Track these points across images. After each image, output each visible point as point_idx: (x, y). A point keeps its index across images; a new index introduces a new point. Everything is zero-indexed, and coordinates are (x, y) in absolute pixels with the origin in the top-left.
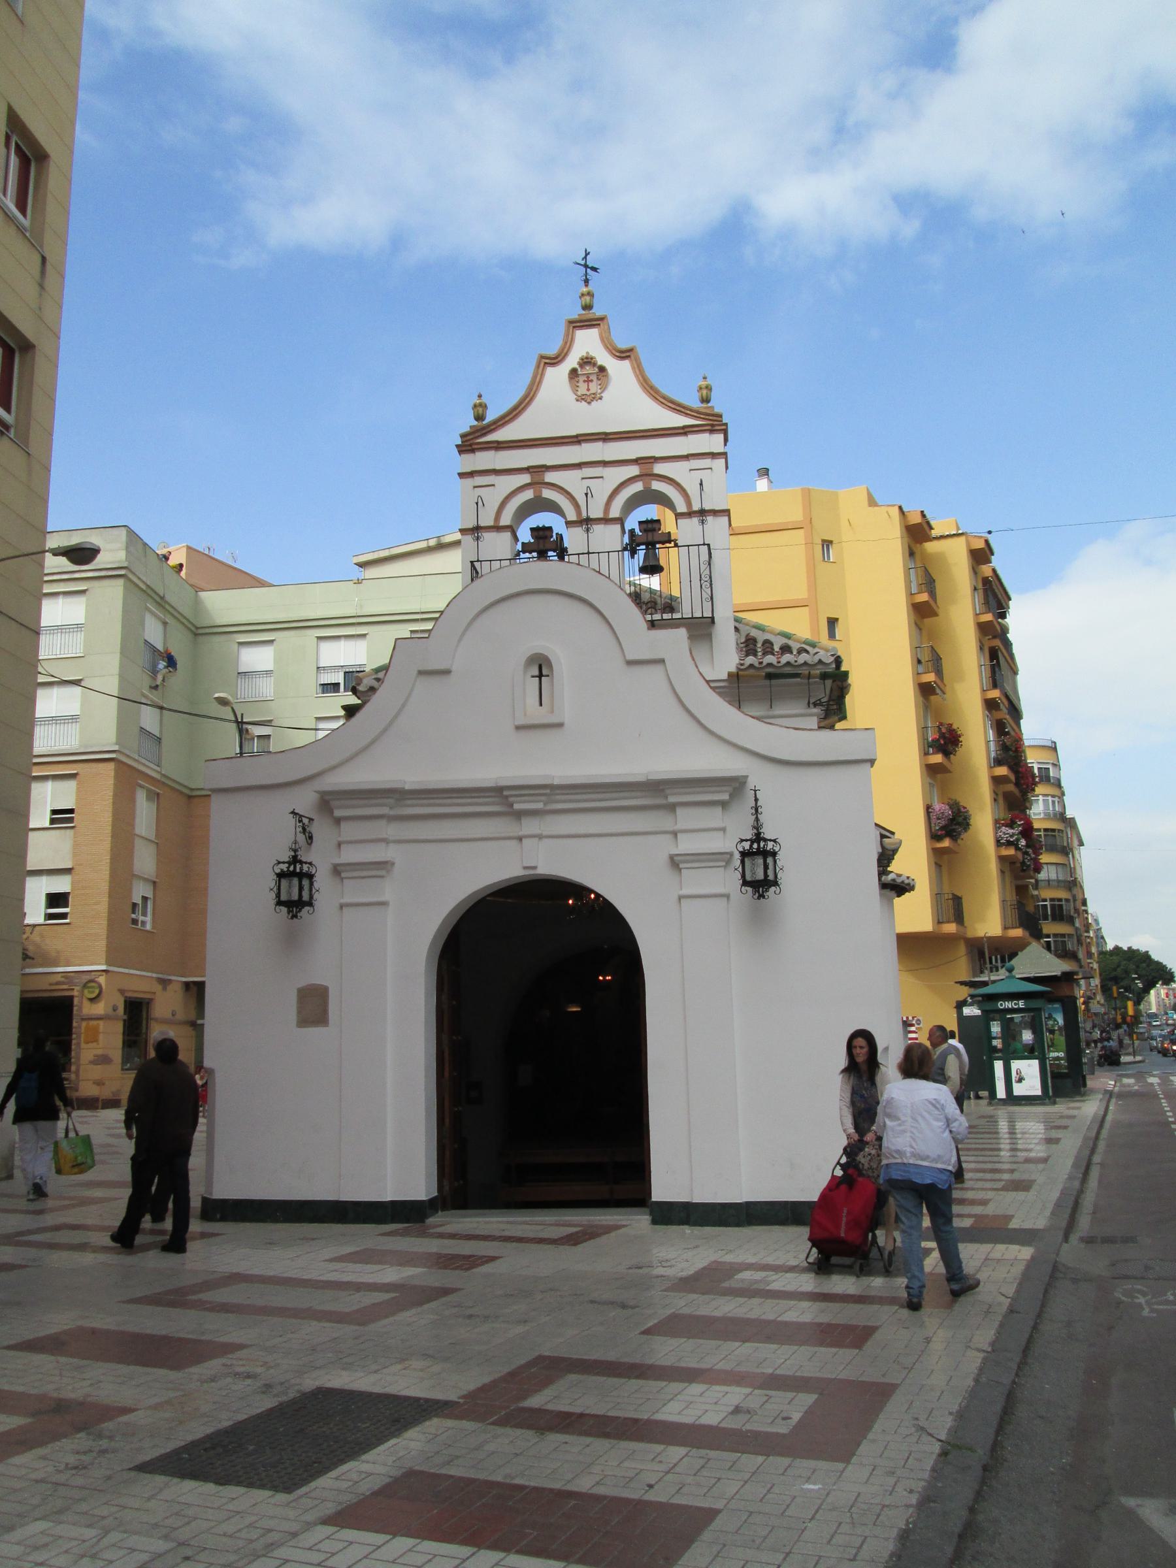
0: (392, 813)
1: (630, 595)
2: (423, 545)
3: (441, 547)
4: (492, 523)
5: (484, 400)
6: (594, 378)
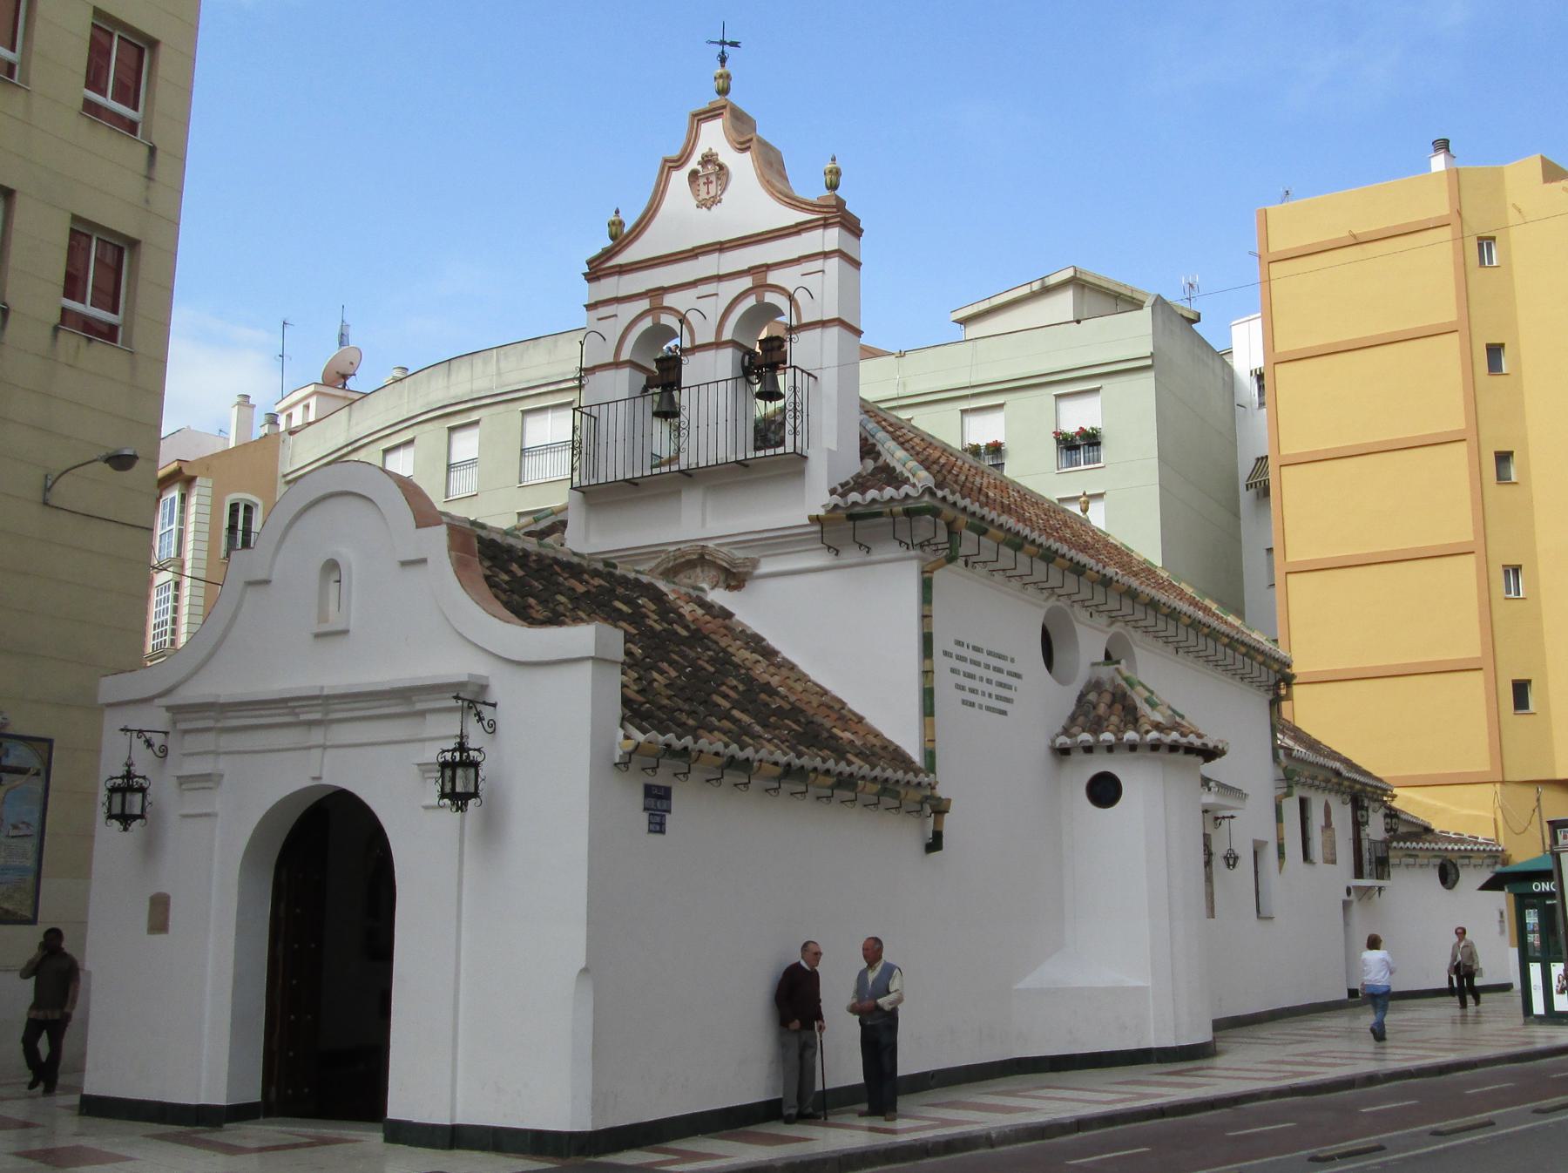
0: (219, 725)
3: (1047, 290)
4: (611, 360)
5: (838, 164)
6: (713, 178)
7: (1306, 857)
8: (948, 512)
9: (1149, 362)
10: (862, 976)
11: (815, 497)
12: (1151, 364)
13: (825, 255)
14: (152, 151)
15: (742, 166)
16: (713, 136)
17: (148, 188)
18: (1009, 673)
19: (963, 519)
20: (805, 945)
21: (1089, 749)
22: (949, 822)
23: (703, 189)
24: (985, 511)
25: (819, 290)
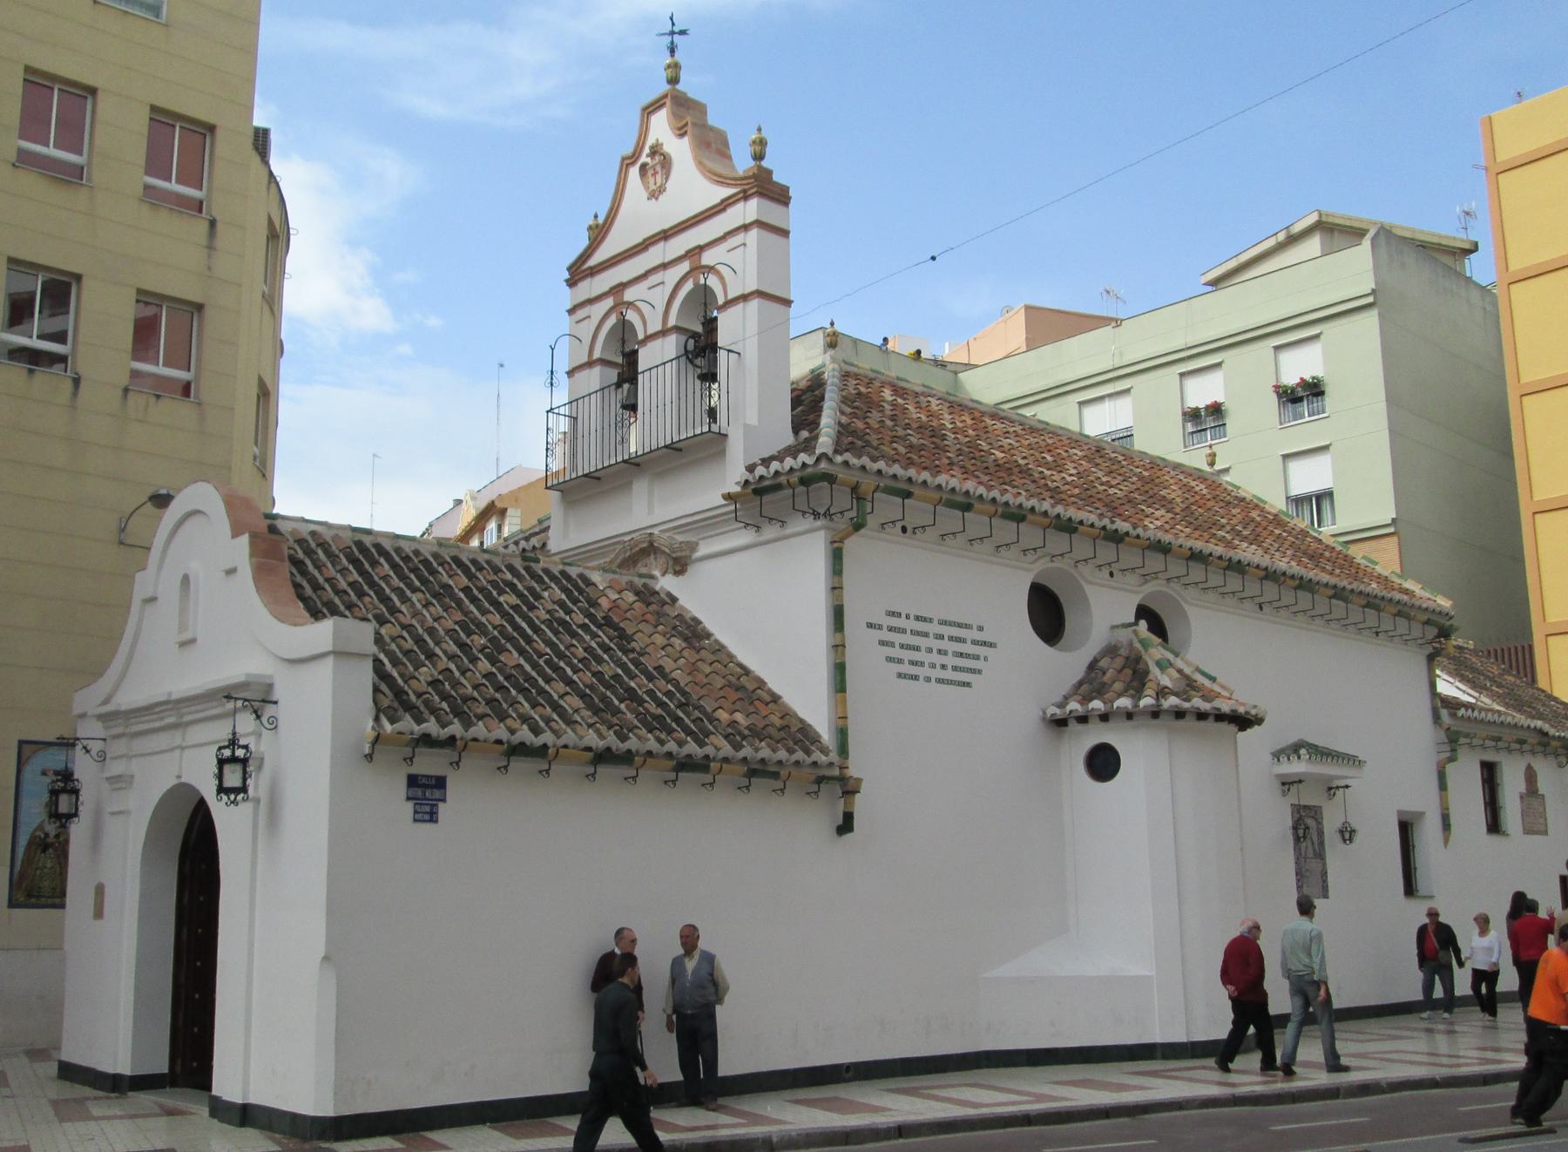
1: (1032, 343)
2: (1271, 243)
3: (1293, 240)
5: (764, 134)
6: (658, 168)
7: (1494, 826)
8: (852, 477)
9: (1370, 299)
10: (677, 964)
11: (732, 475)
12: (1375, 301)
13: (745, 228)
14: (213, 223)
15: (680, 150)
16: (660, 127)
17: (209, 256)
18: (892, 645)
19: (868, 483)
20: (619, 933)
21: (1083, 719)
22: (860, 804)
23: (651, 180)
24: (912, 472)
25: (738, 266)
